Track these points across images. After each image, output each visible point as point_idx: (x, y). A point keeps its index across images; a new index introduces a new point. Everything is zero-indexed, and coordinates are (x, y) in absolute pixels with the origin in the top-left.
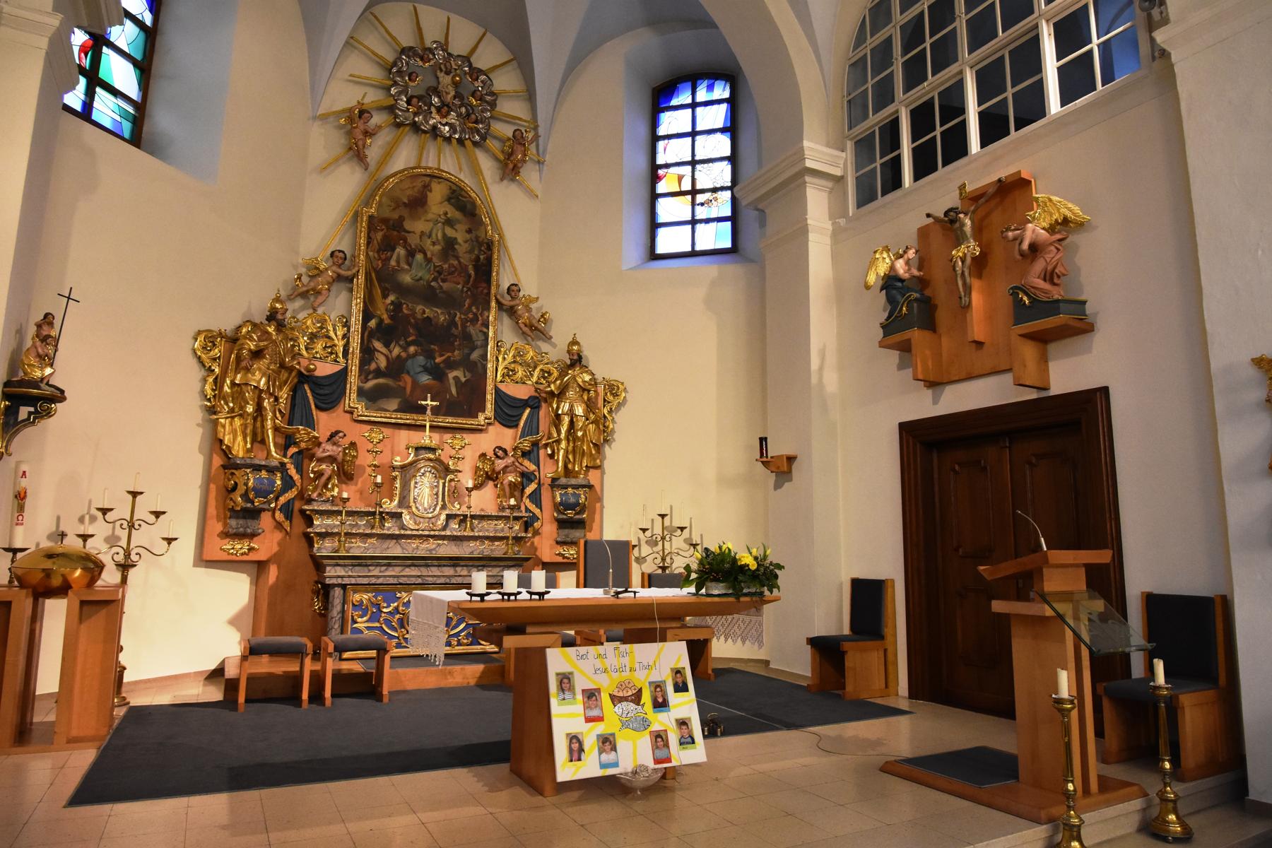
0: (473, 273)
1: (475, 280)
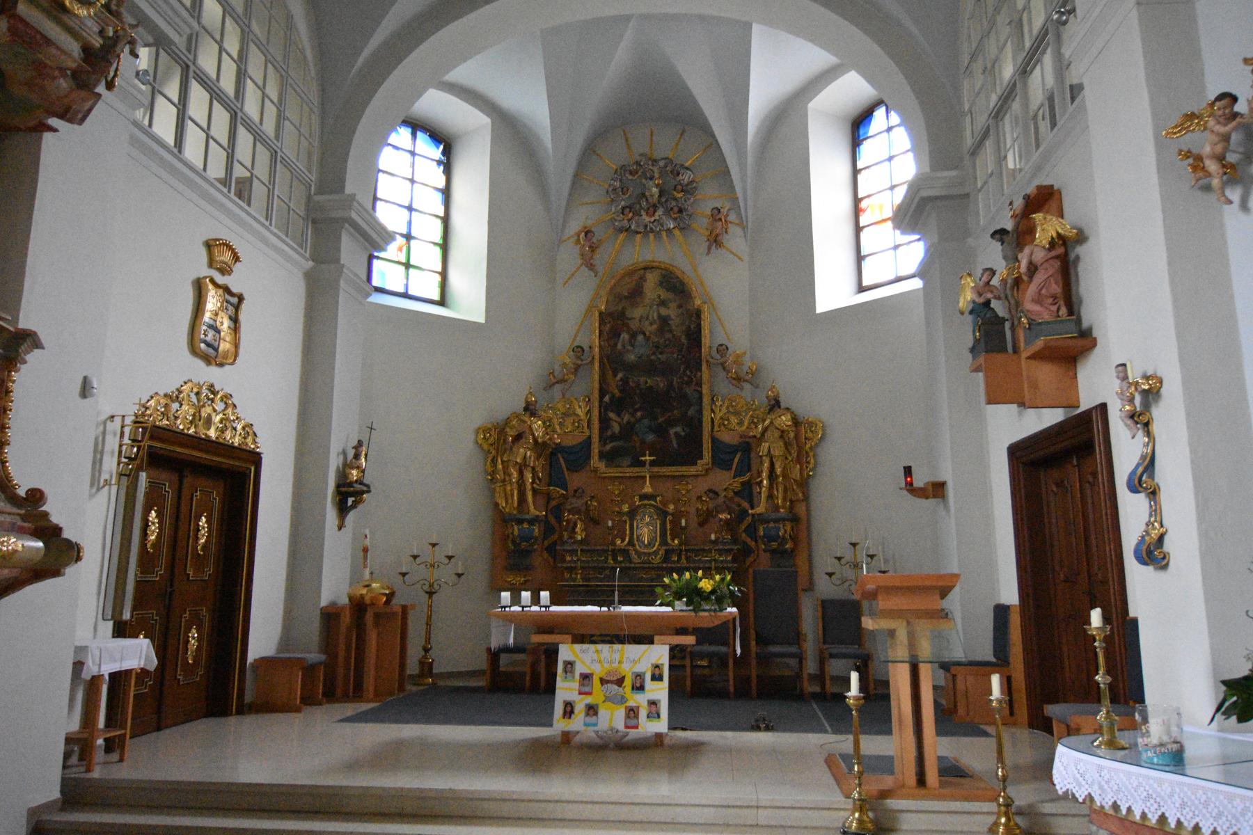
0: (684, 340)
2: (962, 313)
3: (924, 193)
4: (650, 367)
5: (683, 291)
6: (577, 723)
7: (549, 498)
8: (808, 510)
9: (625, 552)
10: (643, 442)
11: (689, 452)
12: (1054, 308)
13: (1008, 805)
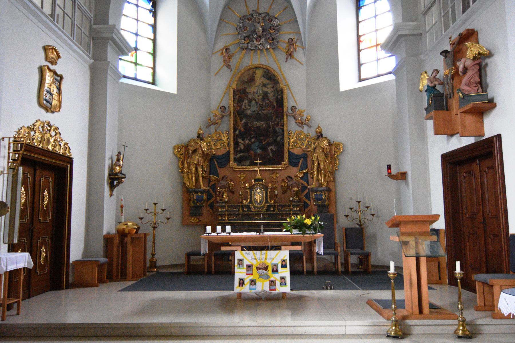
0: (275, 104)
1: (277, 108)
2: (421, 91)
3: (400, 33)
4: (258, 117)
6: (246, 289)
7: (210, 180)
8: (335, 188)
9: (248, 207)
10: (255, 153)
11: (277, 159)
12: (476, 89)
13: (464, 321)
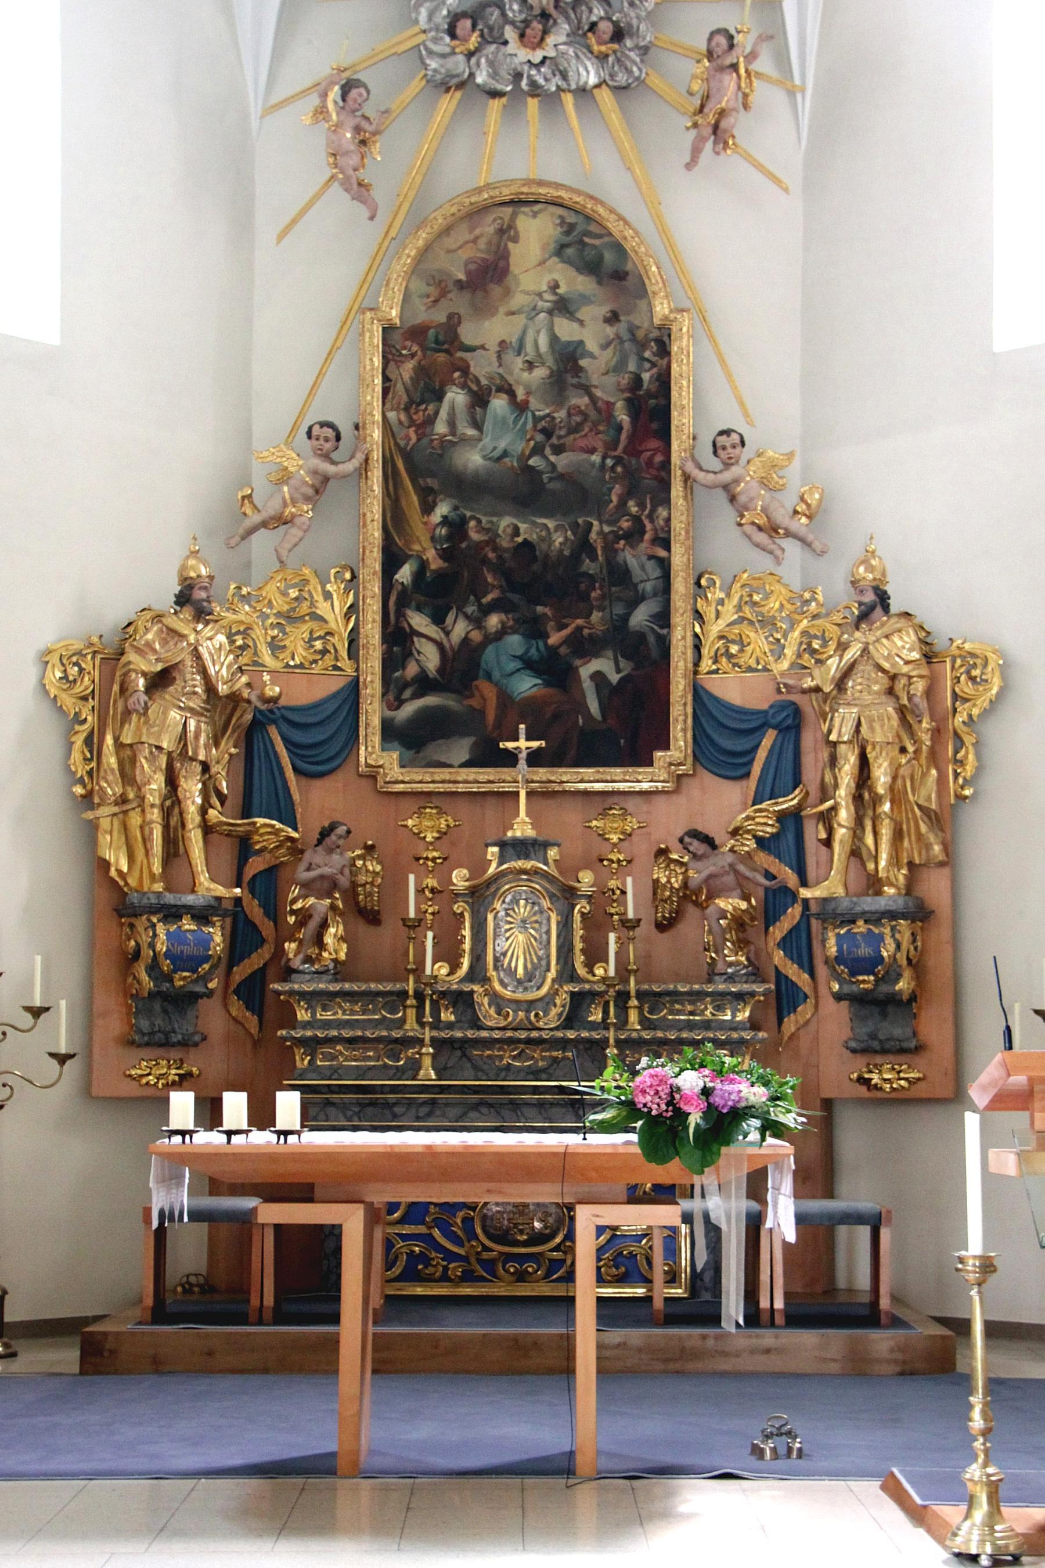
0: (623, 417)
1: (633, 437)
4: (527, 490)
5: (619, 276)
7: (244, 847)
9: (462, 1000)
10: (505, 699)
11: (630, 729)
